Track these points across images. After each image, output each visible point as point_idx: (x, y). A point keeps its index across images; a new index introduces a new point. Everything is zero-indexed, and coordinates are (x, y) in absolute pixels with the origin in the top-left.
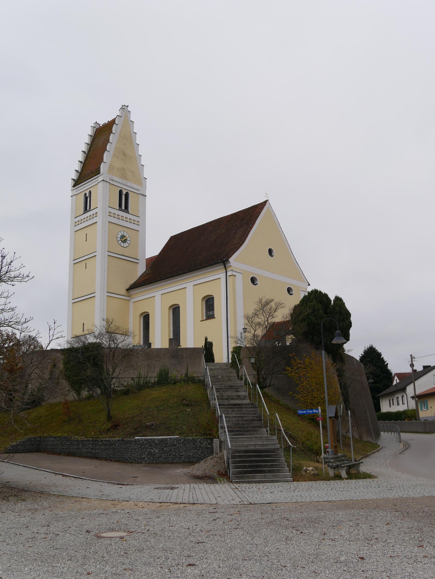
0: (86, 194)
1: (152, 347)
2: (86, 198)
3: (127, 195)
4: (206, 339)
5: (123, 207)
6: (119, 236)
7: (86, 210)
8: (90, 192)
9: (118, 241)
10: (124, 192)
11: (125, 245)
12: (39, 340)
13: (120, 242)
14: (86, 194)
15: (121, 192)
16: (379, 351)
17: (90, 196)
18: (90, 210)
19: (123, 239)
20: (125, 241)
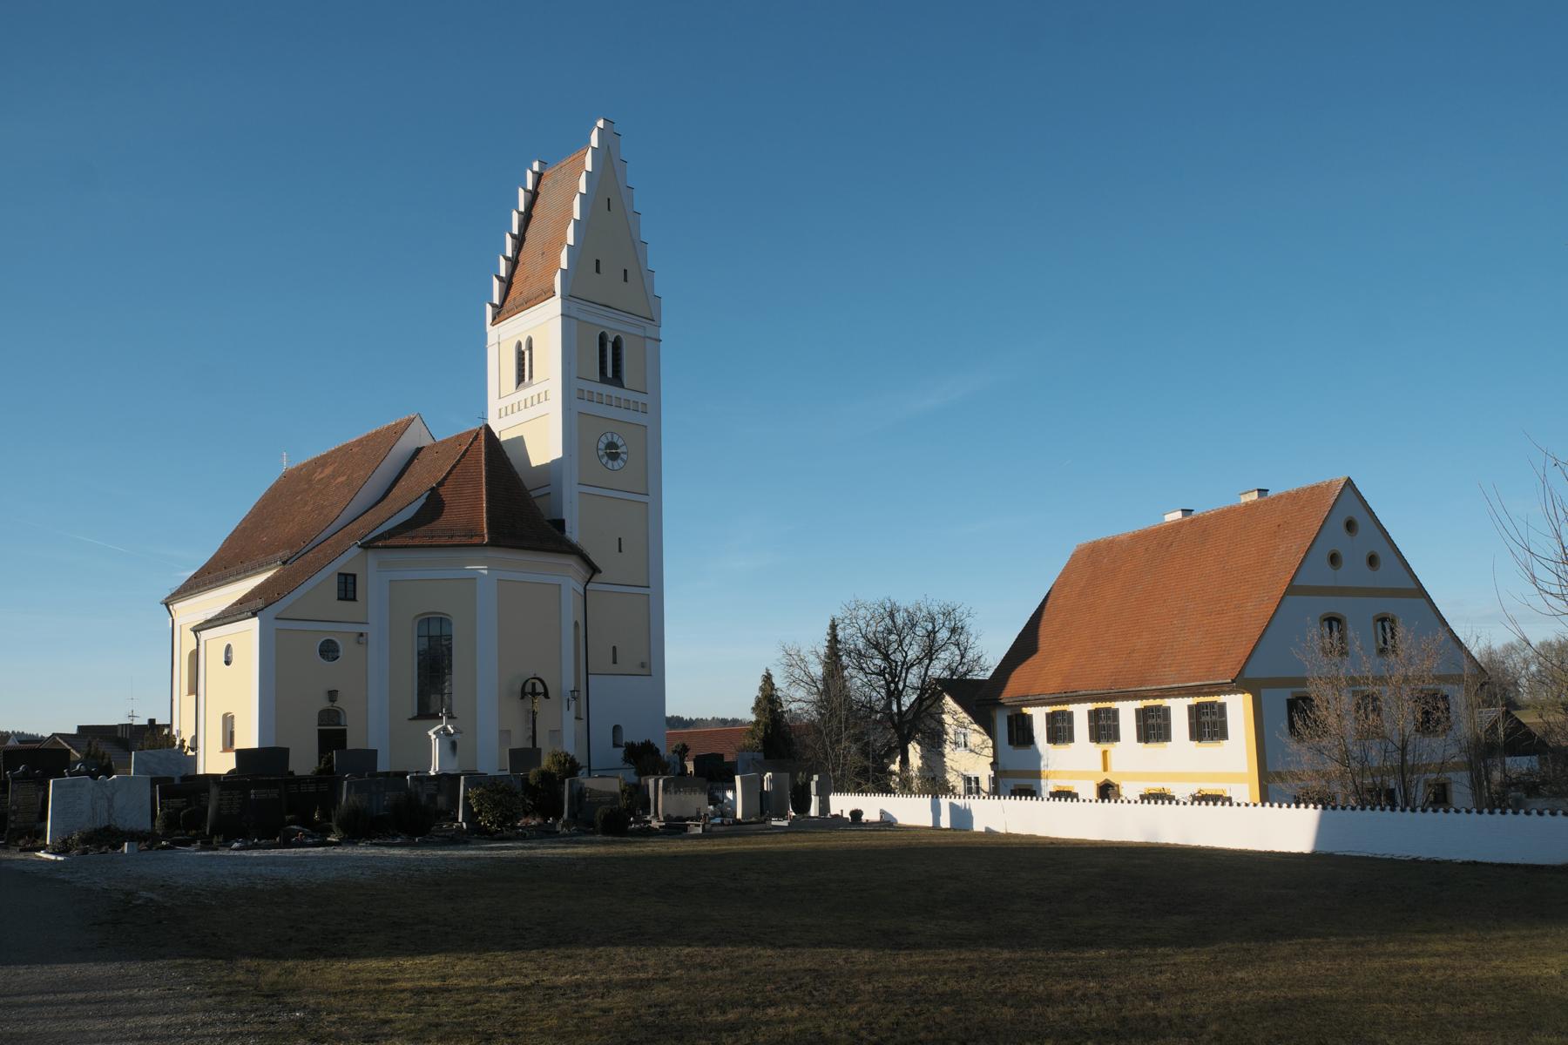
0: (519, 344)
1: (350, 745)
2: (520, 355)
3: (617, 345)
4: (332, 695)
5: (610, 374)
6: (602, 446)
7: (520, 378)
8: (530, 341)
9: (600, 458)
10: (611, 338)
11: (618, 464)
12: (1043, 782)
13: (605, 459)
14: (519, 344)
15: (603, 339)
16: (1150, 745)
17: (530, 348)
18: (530, 384)
19: (612, 452)
20: (614, 457)
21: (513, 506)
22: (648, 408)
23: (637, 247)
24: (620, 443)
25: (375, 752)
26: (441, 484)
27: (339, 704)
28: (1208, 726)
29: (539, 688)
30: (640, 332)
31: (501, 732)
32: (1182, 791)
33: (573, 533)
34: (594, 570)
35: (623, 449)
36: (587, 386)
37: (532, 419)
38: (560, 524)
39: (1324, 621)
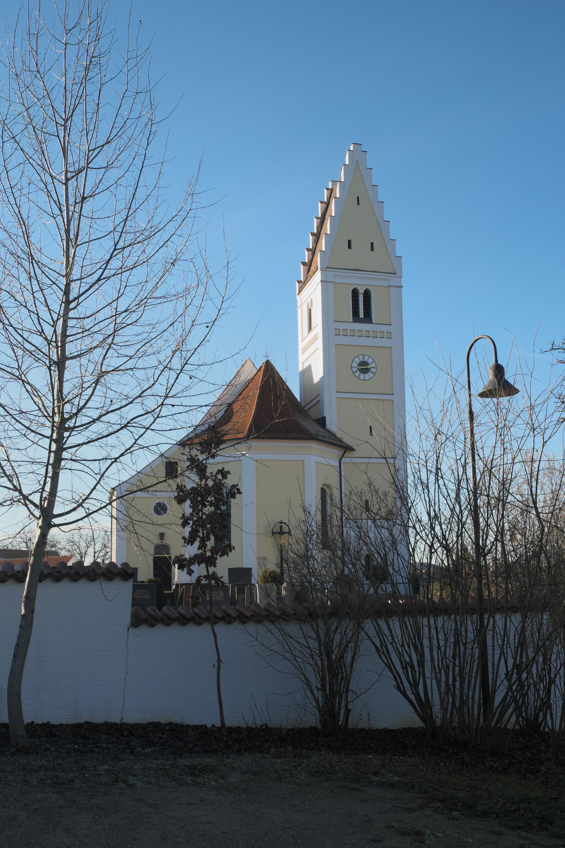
3: (367, 294)
5: (362, 315)
6: (355, 365)
9: (354, 373)
10: (361, 291)
15: (355, 293)
19: (364, 367)
20: (365, 371)
21: (276, 410)
22: (394, 333)
23: (382, 226)
24: (370, 361)
25: (251, 569)
26: (233, 403)
27: (165, 541)
28: (190, 541)
29: (285, 529)
30: (386, 284)
31: (259, 559)
32: (442, 408)
33: (332, 425)
34: (347, 449)
35: (373, 365)
36: (342, 326)
37: (306, 358)
38: (322, 421)
39: (1, 759)
